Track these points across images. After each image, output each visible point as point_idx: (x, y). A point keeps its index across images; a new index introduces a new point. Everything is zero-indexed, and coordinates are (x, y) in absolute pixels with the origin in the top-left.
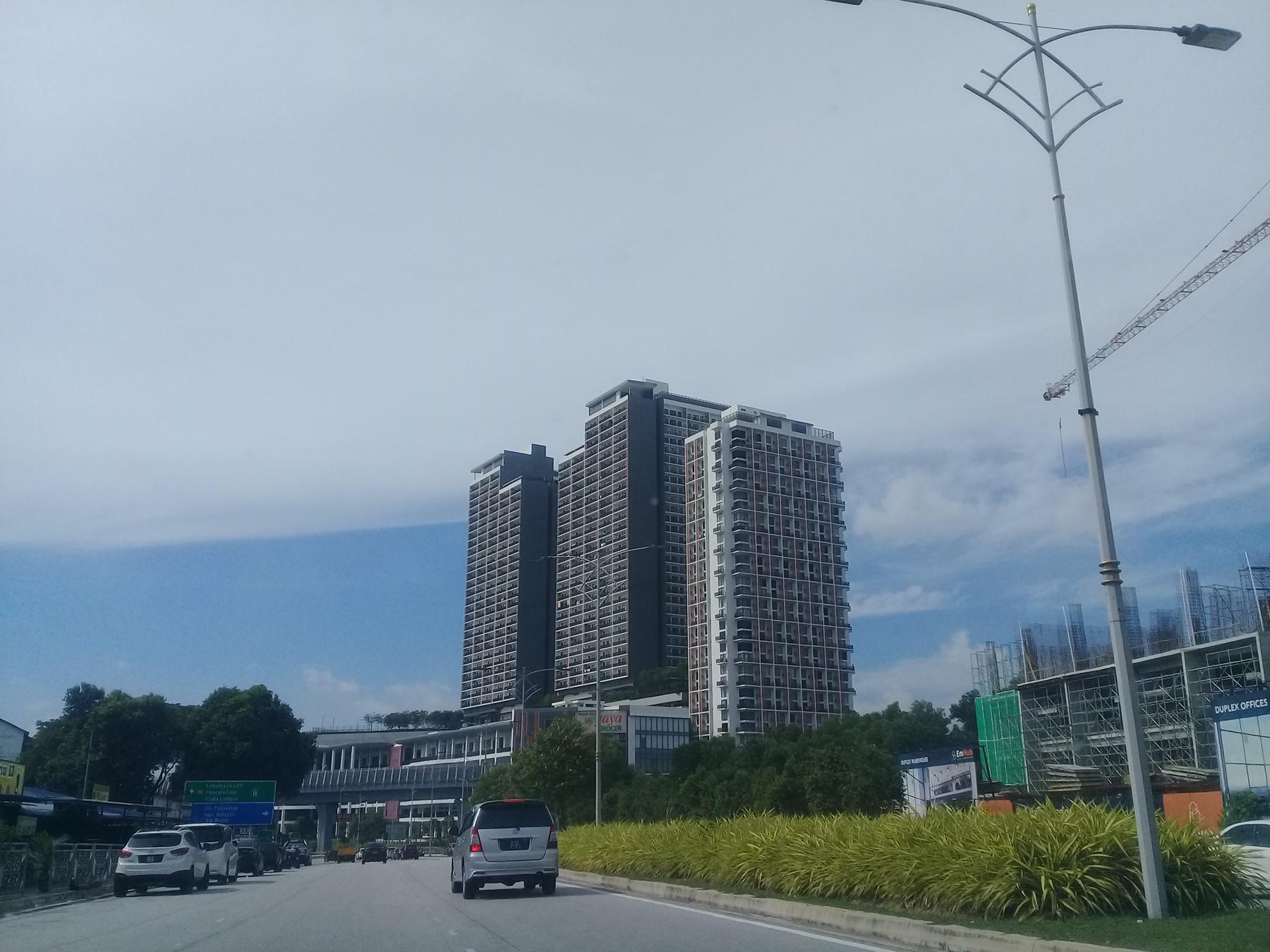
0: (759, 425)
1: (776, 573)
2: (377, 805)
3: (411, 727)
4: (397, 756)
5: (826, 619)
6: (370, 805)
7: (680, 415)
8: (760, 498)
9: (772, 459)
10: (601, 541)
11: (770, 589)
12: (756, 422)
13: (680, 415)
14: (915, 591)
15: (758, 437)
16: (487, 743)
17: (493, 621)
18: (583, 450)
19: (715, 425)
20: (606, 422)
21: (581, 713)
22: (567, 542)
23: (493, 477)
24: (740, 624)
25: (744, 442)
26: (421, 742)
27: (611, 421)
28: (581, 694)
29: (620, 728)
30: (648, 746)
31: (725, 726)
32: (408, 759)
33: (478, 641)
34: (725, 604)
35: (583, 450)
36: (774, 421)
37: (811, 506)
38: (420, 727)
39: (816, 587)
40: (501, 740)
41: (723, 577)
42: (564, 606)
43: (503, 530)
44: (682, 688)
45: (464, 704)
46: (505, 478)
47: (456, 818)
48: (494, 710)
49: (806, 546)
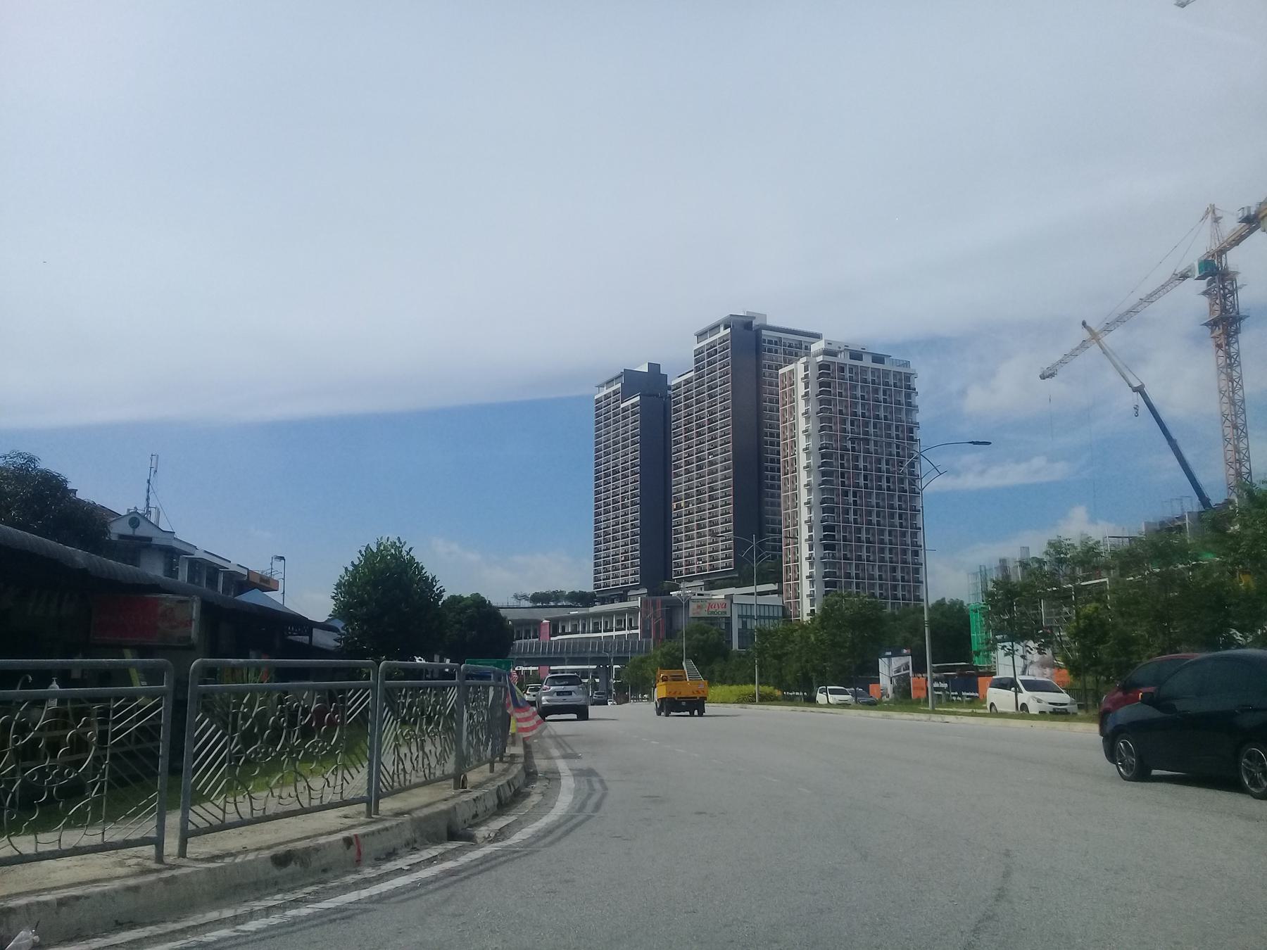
0: (843, 358)
1: (857, 485)
2: (531, 668)
3: (552, 604)
4: (545, 630)
5: (901, 523)
6: (526, 668)
7: (776, 343)
8: (844, 422)
9: (854, 387)
10: (709, 454)
11: (851, 499)
12: (839, 356)
13: (776, 343)
14: (1038, 462)
15: (842, 369)
16: (619, 622)
17: (618, 517)
18: (692, 374)
19: (804, 359)
20: (712, 349)
21: (694, 601)
22: (680, 453)
23: (615, 392)
24: (825, 528)
25: (829, 374)
26: (565, 619)
27: (716, 350)
28: (695, 581)
29: (725, 613)
30: (749, 627)
31: (813, 611)
32: (555, 633)
33: (607, 534)
34: (813, 512)
35: (692, 374)
36: (856, 356)
37: (889, 427)
38: (559, 604)
39: (891, 497)
40: (630, 620)
41: (811, 490)
42: (679, 507)
43: (625, 439)
44: (778, 580)
45: (597, 587)
46: (626, 393)
47: (597, 680)
48: (622, 592)
49: (884, 462)
